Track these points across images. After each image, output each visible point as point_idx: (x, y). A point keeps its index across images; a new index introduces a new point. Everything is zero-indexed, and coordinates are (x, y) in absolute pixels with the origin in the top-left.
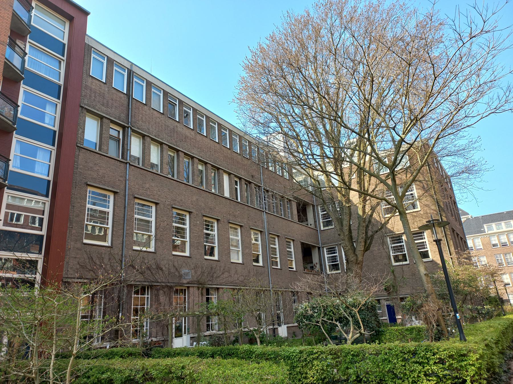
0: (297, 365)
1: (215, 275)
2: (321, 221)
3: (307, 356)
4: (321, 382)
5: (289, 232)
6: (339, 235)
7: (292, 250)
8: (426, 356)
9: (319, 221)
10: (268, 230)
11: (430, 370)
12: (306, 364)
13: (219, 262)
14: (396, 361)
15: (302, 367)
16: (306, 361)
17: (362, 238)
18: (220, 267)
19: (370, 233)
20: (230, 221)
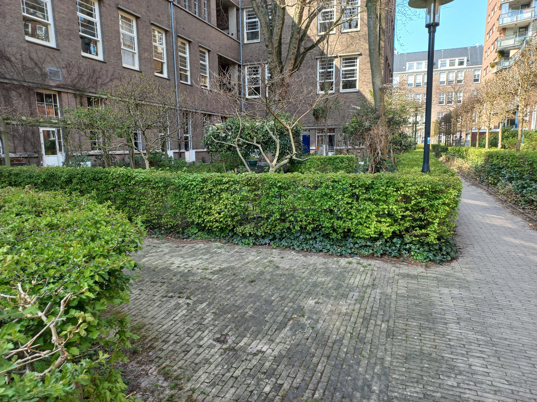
0: (197, 197)
1: (100, 82)
2: (245, 31)
3: (214, 186)
4: (230, 219)
5: (204, 39)
6: (267, 46)
7: (207, 64)
8: (385, 191)
9: (243, 31)
10: (177, 32)
11: (387, 210)
12: (210, 197)
13: (105, 64)
14: (340, 197)
15: (205, 200)
16: (212, 192)
17: (293, 54)
18: (107, 71)
19: (302, 50)
20: (120, 6)
